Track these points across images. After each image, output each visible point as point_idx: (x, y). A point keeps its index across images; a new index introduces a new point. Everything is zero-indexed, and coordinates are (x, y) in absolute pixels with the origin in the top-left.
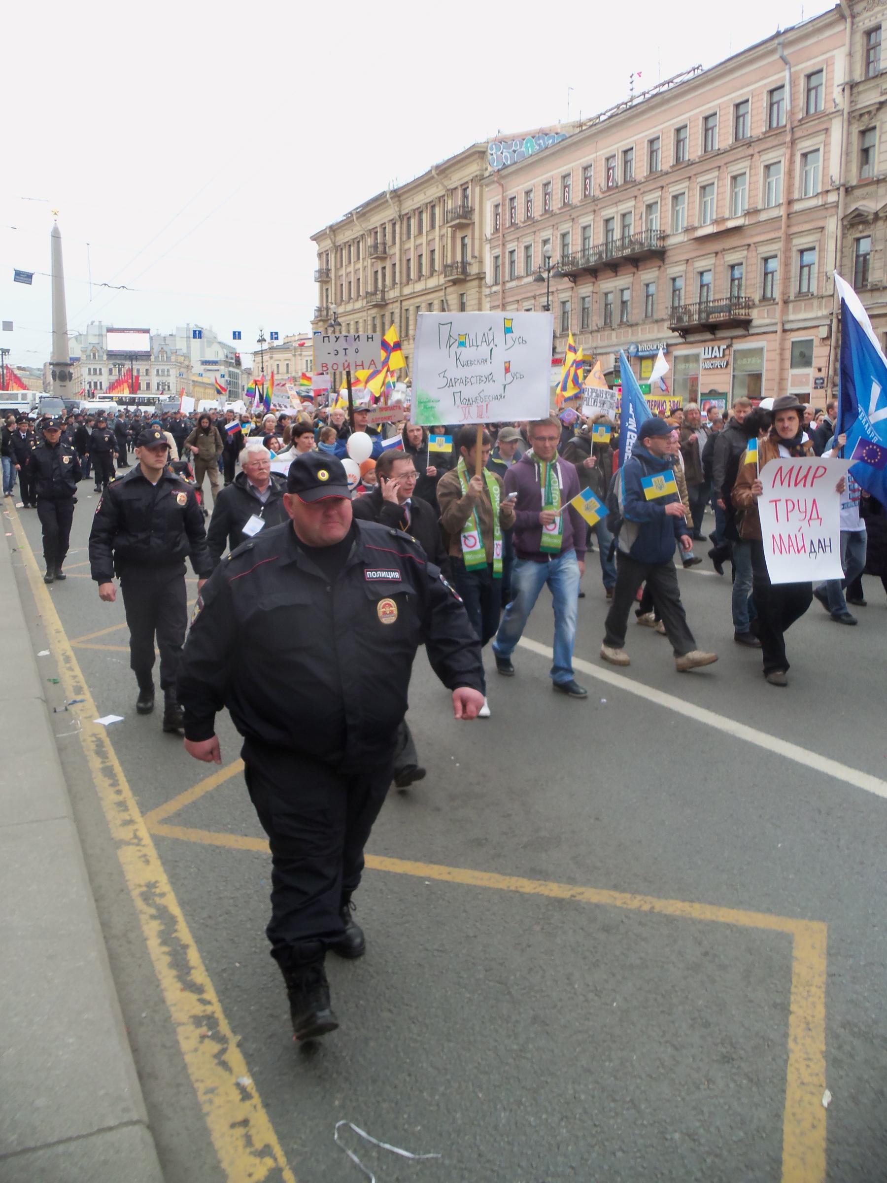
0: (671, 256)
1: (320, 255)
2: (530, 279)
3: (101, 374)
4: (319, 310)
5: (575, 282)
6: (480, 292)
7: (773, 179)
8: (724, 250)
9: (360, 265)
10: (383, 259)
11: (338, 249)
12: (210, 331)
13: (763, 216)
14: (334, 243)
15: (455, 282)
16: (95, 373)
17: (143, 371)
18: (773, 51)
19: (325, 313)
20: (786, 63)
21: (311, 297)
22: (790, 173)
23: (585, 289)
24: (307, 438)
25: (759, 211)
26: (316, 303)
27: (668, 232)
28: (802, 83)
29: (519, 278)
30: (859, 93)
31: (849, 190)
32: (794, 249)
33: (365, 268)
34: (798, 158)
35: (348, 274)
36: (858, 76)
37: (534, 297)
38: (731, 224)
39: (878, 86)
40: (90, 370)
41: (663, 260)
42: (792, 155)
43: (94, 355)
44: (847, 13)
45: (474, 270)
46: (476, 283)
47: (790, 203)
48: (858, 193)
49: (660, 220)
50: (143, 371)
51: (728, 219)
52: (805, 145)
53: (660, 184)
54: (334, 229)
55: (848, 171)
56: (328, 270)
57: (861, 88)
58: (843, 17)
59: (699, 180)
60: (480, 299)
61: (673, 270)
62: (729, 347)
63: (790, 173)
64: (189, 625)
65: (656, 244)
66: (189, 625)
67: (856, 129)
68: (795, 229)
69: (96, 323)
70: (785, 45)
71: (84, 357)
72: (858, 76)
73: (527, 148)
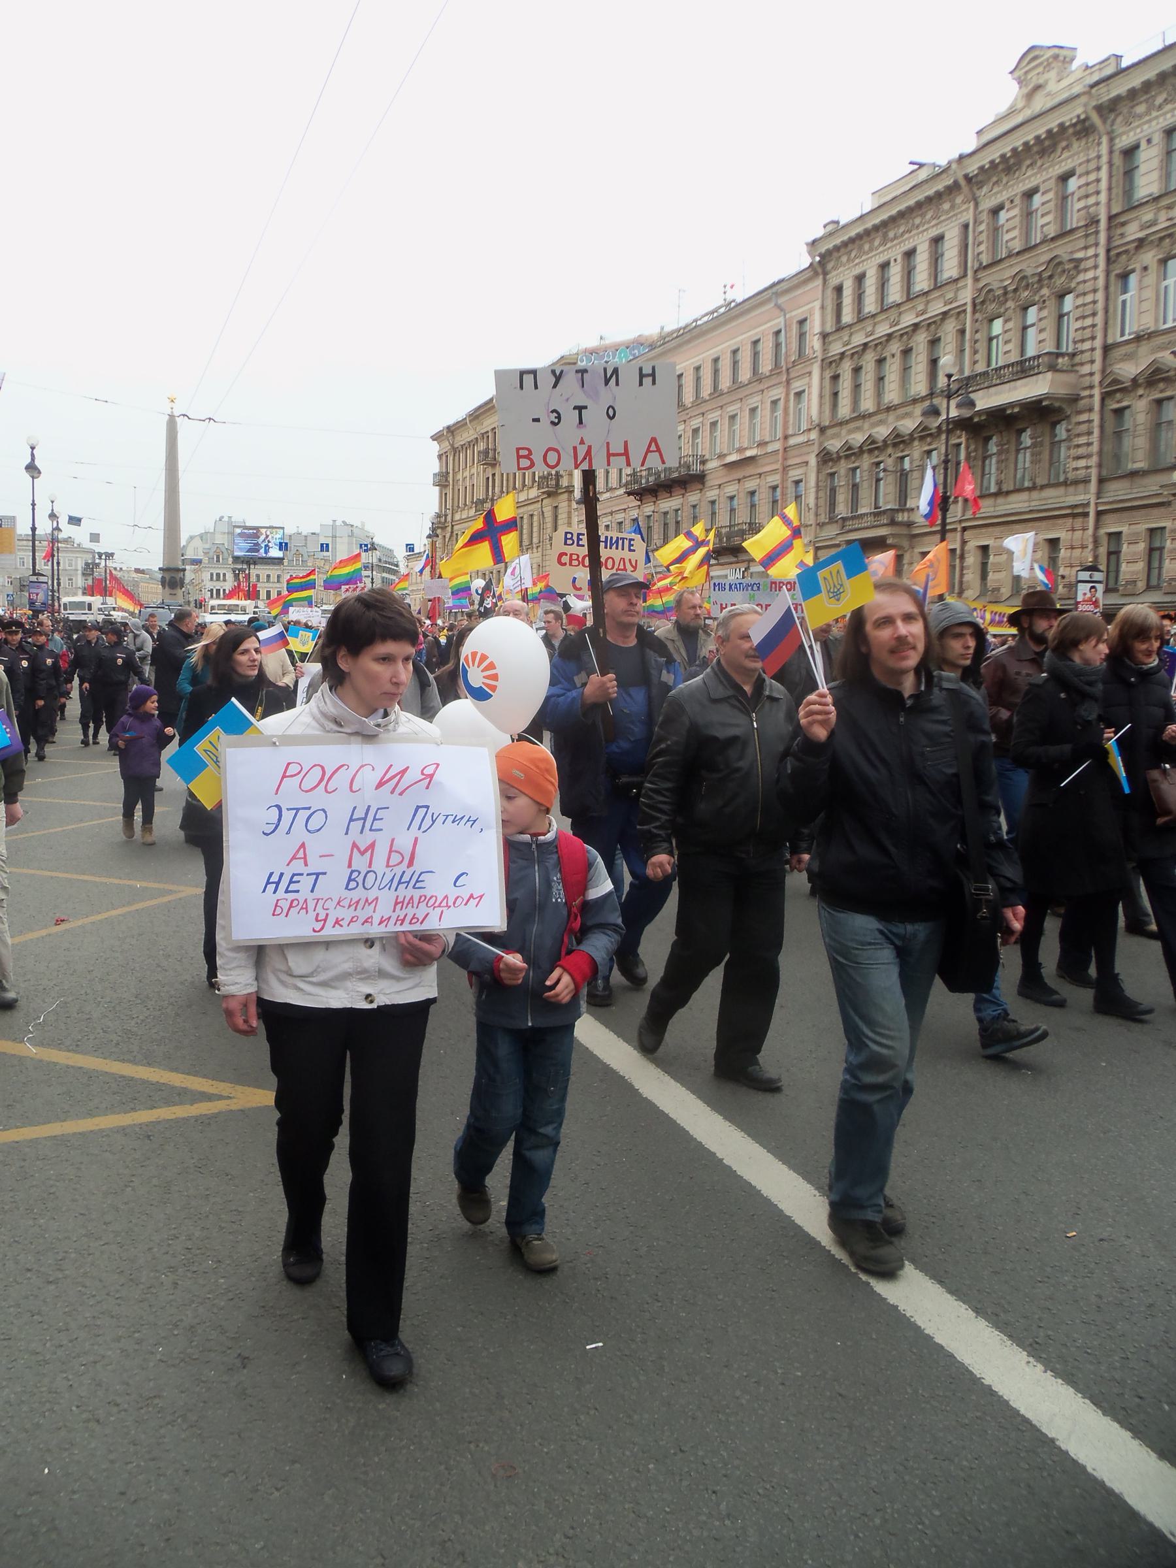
0: (711, 481)
1: (440, 457)
2: (622, 491)
3: (225, 580)
4: (438, 516)
5: (641, 500)
6: (570, 506)
7: (737, 427)
8: (745, 477)
9: (474, 471)
10: (493, 465)
11: (455, 450)
12: (362, 529)
13: (770, 448)
14: (452, 446)
15: (550, 494)
16: (218, 579)
17: (263, 578)
18: (769, 300)
19: (443, 520)
20: (782, 310)
21: (430, 502)
22: (786, 409)
23: (648, 509)
24: (387, 659)
25: (767, 443)
26: (435, 508)
27: (707, 457)
28: (795, 328)
29: (612, 489)
30: (830, 343)
31: (823, 430)
32: (790, 480)
33: (478, 474)
34: (792, 397)
35: (464, 479)
36: (829, 328)
37: (611, 513)
38: (749, 453)
39: (841, 338)
40: (212, 575)
41: (703, 484)
42: (787, 395)
43: (218, 557)
44: (820, 270)
45: (564, 482)
46: (565, 496)
47: (786, 437)
48: (830, 432)
49: (704, 448)
50: (263, 578)
51: (746, 449)
52: (797, 385)
53: (701, 411)
54: (451, 430)
55: (821, 412)
56: (448, 473)
57: (831, 338)
58: (816, 274)
59: (729, 409)
60: (569, 513)
61: (712, 494)
62: (747, 569)
63: (786, 409)
64: (723, 964)
65: (696, 468)
66: (723, 964)
67: (828, 374)
68: (790, 462)
69: (226, 519)
70: (778, 295)
71: (205, 560)
72: (829, 328)
73: (620, 358)
